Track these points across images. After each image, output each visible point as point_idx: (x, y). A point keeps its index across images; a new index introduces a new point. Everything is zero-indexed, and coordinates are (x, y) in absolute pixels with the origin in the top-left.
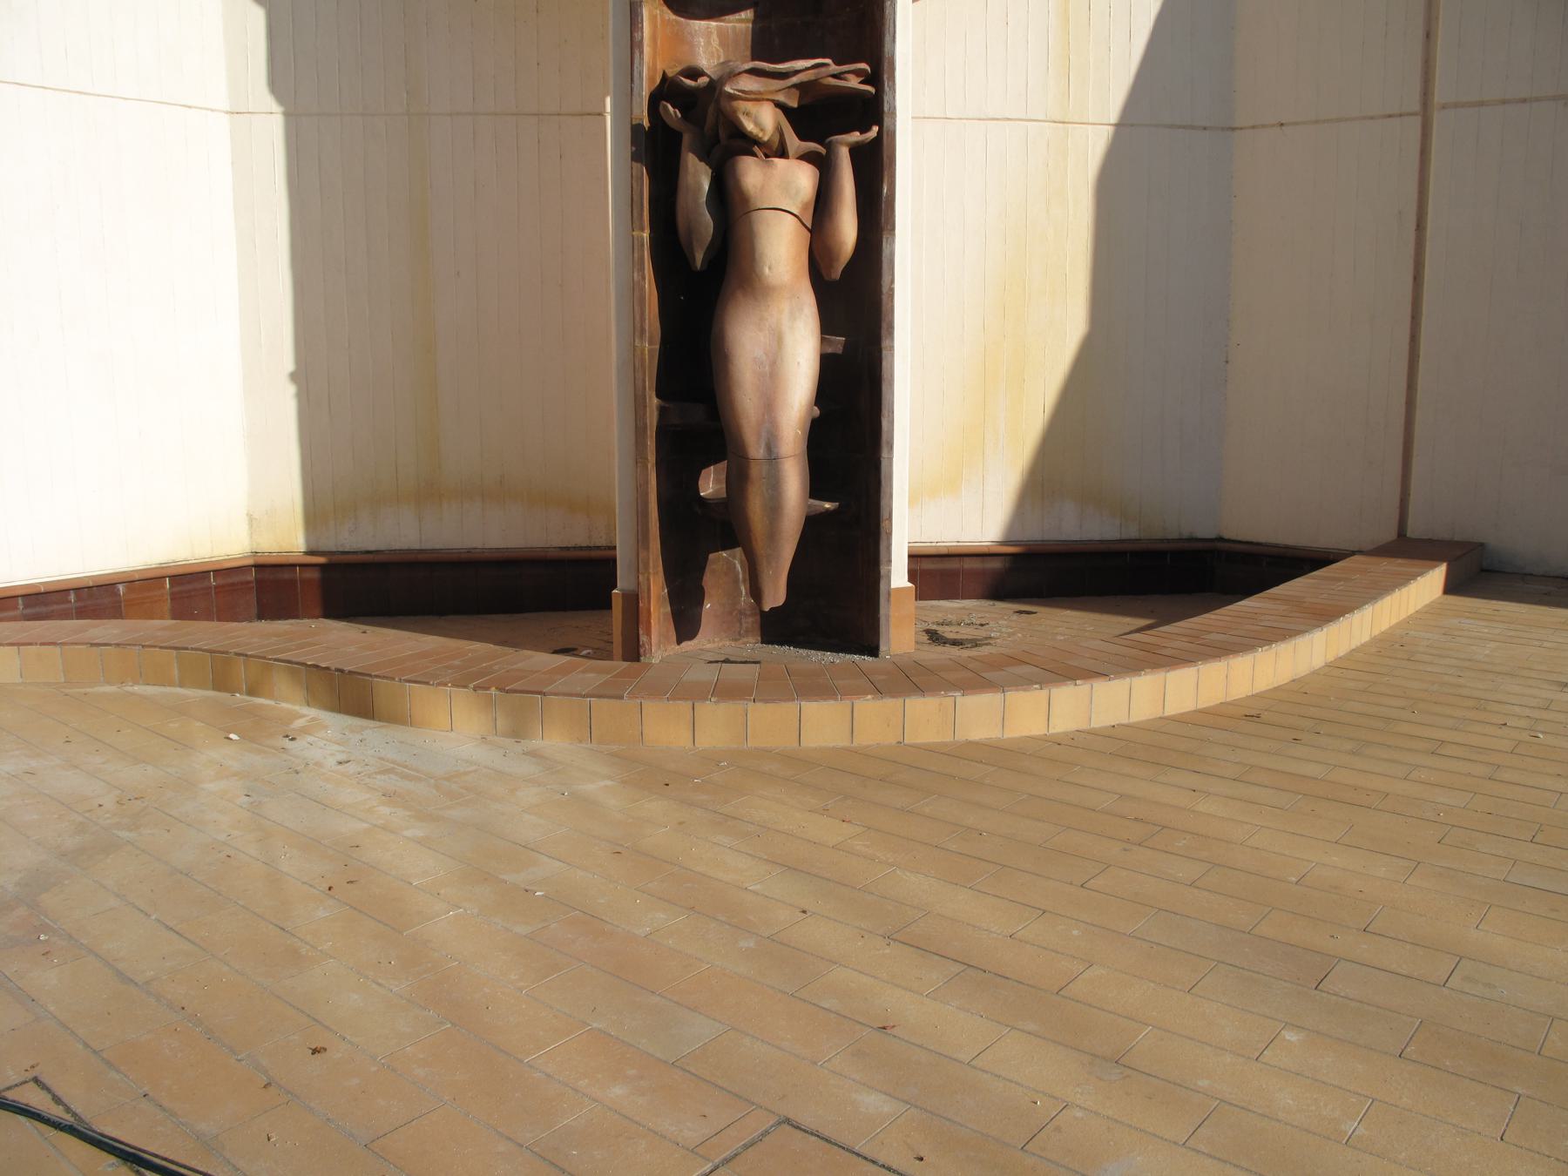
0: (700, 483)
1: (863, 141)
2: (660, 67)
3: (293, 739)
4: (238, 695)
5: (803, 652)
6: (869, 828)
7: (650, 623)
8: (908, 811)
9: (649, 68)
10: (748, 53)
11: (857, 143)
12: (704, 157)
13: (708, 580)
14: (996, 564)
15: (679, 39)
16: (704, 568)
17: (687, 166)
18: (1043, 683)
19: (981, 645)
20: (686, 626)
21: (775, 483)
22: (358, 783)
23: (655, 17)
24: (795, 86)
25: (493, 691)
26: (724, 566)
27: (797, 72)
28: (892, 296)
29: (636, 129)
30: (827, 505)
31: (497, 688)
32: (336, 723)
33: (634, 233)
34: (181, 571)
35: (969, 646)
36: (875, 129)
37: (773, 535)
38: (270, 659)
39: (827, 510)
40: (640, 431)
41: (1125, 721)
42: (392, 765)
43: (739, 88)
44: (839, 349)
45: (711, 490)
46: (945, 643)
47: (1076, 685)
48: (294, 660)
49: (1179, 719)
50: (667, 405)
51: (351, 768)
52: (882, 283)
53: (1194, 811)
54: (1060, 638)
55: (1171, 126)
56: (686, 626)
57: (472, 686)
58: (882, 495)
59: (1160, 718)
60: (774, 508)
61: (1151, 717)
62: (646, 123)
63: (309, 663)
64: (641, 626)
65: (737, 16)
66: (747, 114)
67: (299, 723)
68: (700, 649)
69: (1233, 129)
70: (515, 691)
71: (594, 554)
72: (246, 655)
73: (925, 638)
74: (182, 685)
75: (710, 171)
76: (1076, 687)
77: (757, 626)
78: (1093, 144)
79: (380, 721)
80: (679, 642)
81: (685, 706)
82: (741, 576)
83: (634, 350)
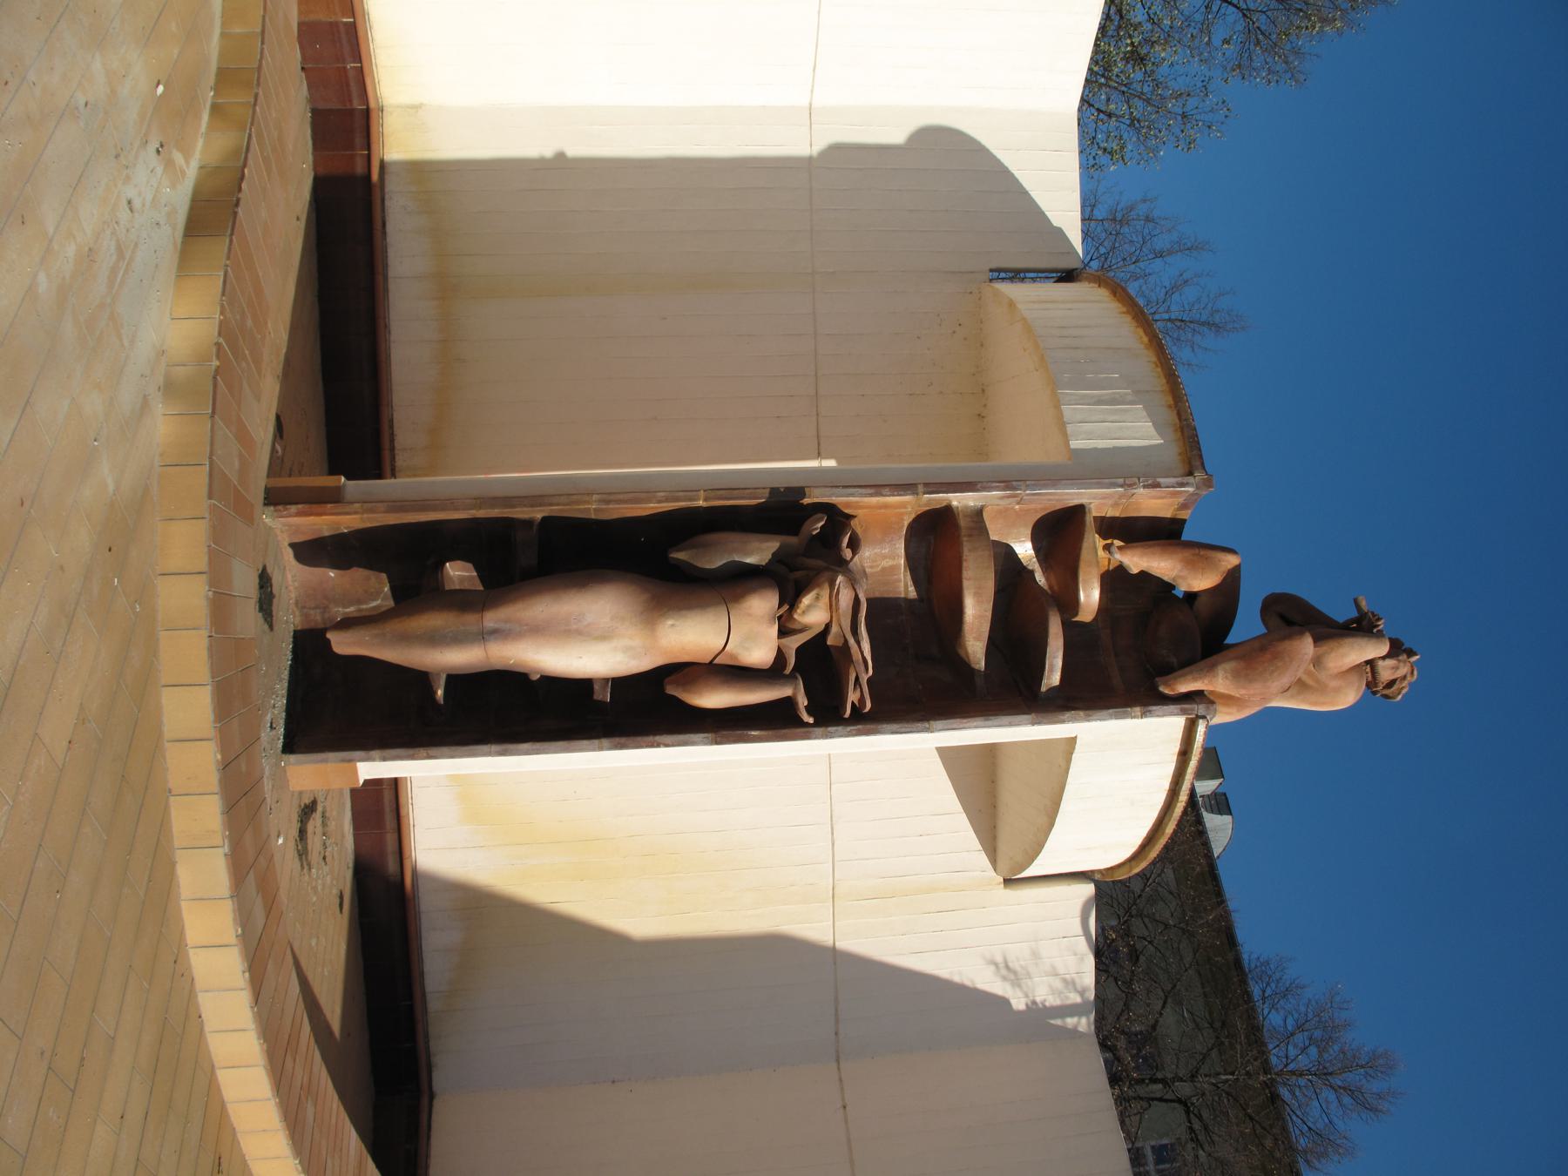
0: (459, 562)
1: (799, 709)
2: (859, 512)
3: (158, 152)
4: (212, 94)
5: (285, 675)
6: (61, 770)
7: (311, 515)
8: (85, 809)
9: (857, 502)
10: (872, 596)
11: (797, 704)
12: (777, 558)
13: (358, 574)
14: (392, 866)
15: (887, 530)
16: (371, 568)
17: (767, 541)
18: (244, 938)
19: (301, 859)
20: (311, 552)
21: (458, 639)
22: (104, 222)
23: (905, 508)
24: (846, 641)
25: (216, 363)
26: (375, 589)
27: (858, 643)
28: (652, 746)
29: (800, 492)
30: (440, 692)
31: (218, 367)
32: (180, 197)
33: (702, 492)
34: (361, 33)
35: (300, 847)
36: (811, 720)
37: (406, 639)
38: (251, 129)
39: (436, 693)
40: (508, 501)
41: (207, 1029)
42: (128, 257)
43: (841, 590)
44: (598, 696)
45: (452, 573)
46: (302, 821)
47: (244, 972)
48: (250, 156)
49: (212, 1086)
50: (535, 528)
51: (124, 214)
52: (665, 736)
53: (95, 1121)
54: (314, 942)
55: (836, 1000)
56: (311, 552)
57: (221, 340)
58: (453, 748)
59: (213, 1066)
60: (435, 639)
61: (213, 1055)
62: (806, 501)
63: (246, 171)
64: (306, 506)
65: (910, 582)
66: (817, 598)
67: (178, 157)
68: (285, 567)
69: (838, 1061)
70: (215, 385)
71: (386, 454)
72: (255, 105)
73: (307, 801)
74: (223, 35)
75: (764, 564)
76: (241, 973)
77: (312, 625)
78: (814, 927)
79: (182, 242)
80: (293, 546)
81: (203, 564)
82: (364, 607)
83: (588, 494)
